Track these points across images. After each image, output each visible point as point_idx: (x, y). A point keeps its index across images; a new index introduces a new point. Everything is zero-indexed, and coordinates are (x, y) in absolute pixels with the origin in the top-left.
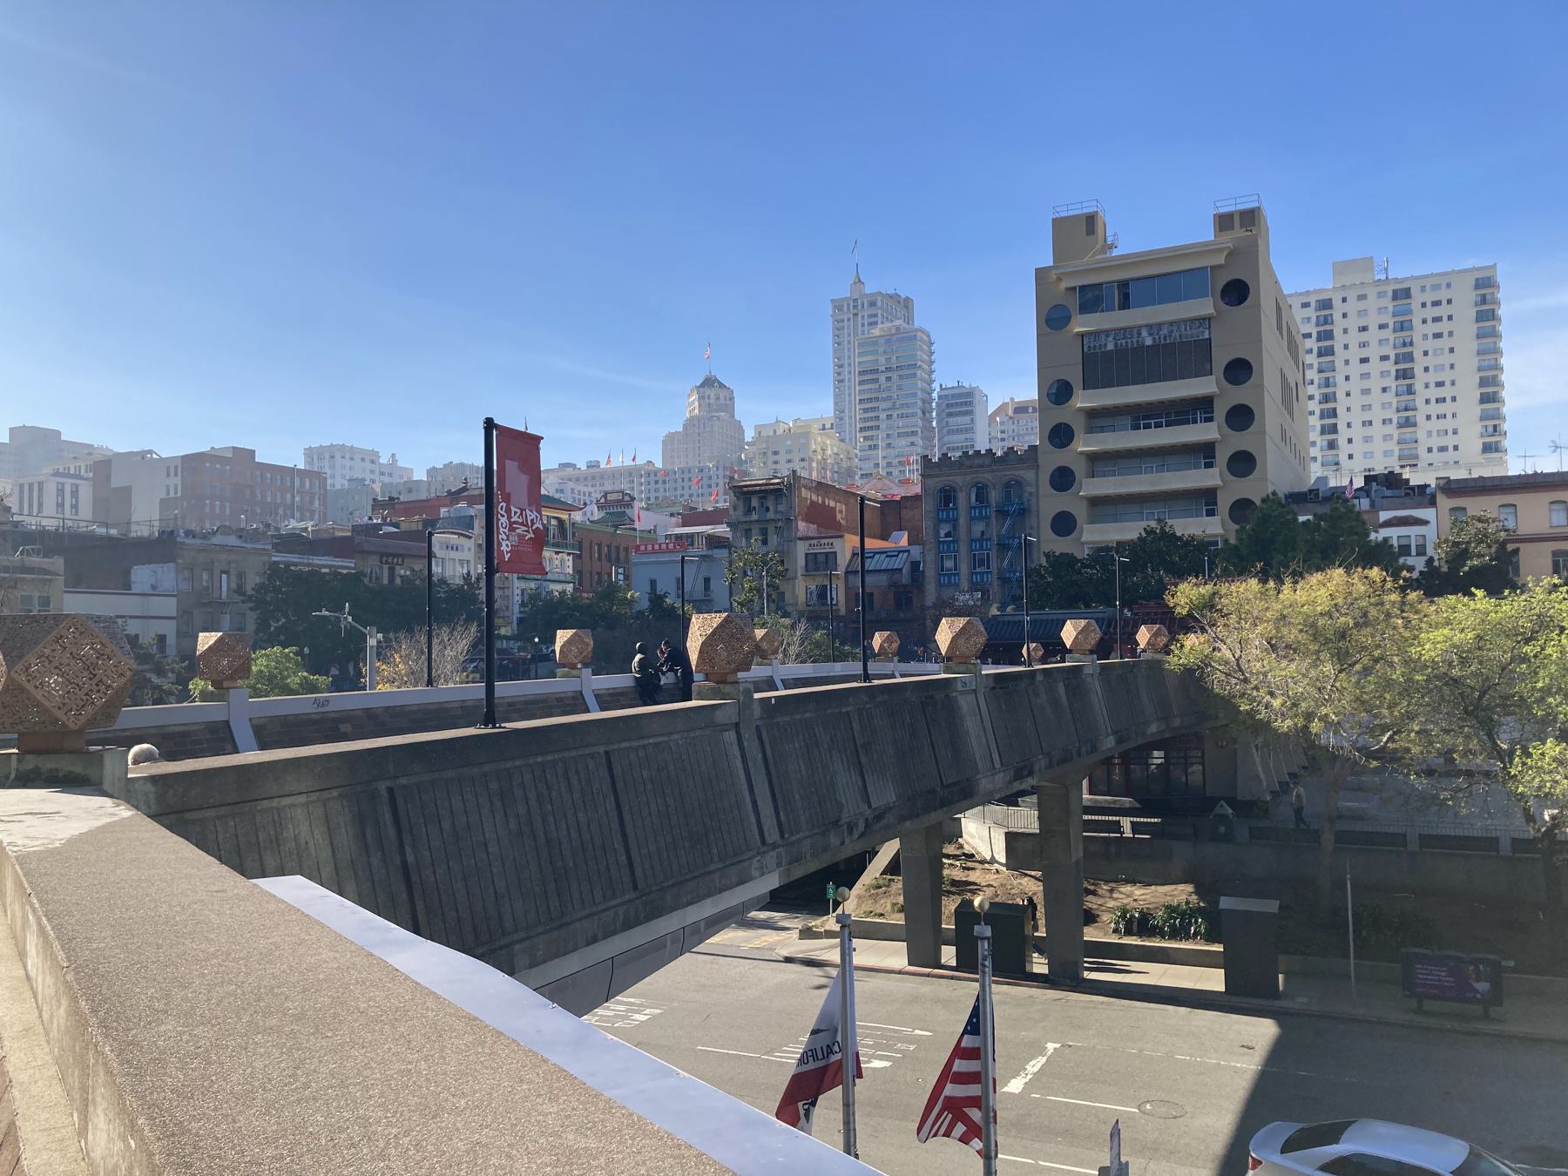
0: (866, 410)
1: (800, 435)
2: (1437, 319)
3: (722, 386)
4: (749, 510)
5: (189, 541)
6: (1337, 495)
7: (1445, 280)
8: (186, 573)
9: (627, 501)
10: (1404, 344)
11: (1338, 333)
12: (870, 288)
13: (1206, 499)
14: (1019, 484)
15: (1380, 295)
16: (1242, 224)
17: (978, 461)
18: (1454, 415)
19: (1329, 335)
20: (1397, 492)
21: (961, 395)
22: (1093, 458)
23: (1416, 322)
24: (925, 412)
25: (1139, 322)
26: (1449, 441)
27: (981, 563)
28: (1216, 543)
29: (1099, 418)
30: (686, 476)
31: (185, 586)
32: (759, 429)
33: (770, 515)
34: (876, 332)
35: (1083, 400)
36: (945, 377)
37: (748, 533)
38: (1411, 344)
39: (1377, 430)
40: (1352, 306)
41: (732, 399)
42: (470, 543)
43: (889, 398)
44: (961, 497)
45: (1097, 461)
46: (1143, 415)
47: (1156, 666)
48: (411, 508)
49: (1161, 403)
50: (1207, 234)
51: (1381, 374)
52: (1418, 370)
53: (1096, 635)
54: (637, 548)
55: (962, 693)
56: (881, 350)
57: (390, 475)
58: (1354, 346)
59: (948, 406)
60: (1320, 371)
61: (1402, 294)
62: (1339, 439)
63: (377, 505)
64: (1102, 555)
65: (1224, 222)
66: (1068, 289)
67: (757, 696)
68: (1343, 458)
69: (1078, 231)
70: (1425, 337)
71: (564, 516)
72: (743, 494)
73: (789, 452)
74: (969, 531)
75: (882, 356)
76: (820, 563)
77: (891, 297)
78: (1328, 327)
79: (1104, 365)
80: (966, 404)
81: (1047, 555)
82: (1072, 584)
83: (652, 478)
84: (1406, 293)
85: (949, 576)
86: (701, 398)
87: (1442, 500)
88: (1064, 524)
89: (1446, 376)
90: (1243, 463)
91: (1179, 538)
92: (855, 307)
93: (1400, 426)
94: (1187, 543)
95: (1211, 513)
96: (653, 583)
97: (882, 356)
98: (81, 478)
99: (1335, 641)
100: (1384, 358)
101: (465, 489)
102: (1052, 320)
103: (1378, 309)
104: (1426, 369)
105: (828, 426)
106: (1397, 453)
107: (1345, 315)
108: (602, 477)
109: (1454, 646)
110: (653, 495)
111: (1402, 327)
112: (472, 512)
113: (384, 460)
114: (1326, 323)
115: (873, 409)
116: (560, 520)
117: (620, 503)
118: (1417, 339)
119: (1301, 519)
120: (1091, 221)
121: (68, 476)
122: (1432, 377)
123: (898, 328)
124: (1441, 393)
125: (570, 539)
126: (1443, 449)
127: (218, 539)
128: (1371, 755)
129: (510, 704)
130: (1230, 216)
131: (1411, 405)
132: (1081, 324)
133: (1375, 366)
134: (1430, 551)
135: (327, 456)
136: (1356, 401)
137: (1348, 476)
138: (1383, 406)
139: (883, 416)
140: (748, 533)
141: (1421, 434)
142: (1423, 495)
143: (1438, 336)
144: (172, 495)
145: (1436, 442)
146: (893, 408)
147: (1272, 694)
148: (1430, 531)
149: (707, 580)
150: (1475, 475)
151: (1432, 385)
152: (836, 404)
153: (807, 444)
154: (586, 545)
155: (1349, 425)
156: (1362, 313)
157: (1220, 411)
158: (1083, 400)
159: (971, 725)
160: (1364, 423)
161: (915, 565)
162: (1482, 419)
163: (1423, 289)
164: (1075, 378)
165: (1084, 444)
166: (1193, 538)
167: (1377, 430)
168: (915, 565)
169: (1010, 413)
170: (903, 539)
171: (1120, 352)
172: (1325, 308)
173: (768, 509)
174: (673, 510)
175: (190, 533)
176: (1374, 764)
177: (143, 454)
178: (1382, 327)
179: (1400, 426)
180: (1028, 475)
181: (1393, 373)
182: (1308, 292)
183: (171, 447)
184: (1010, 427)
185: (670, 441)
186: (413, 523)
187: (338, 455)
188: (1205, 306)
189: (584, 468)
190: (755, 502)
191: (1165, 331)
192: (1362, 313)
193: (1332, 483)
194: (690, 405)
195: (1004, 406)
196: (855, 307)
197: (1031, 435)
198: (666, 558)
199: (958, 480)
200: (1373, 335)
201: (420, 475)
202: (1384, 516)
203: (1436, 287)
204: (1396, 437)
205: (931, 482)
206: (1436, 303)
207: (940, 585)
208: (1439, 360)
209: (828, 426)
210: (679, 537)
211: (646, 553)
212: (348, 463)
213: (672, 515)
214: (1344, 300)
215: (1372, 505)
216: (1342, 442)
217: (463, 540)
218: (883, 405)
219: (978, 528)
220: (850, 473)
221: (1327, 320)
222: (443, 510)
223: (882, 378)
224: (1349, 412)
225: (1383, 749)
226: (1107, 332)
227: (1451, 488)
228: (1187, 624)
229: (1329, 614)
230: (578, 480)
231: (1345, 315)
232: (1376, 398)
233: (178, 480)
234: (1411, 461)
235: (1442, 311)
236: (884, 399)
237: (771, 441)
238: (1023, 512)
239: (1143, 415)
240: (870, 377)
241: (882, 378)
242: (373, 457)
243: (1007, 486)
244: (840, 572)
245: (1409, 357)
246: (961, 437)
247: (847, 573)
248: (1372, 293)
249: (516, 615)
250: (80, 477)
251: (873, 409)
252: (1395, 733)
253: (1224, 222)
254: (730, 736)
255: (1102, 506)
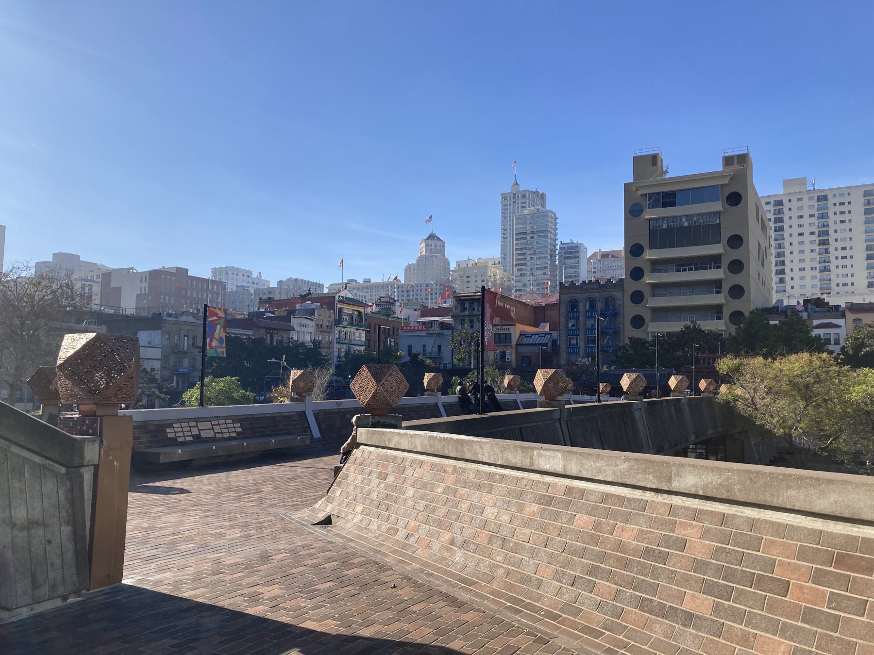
0: (519, 255)
1: (481, 267)
2: (842, 213)
3: (438, 239)
4: (464, 309)
5: (169, 319)
6: (792, 308)
7: (847, 191)
8: (167, 336)
9: (391, 302)
10: (824, 226)
11: (786, 218)
12: (522, 188)
13: (717, 311)
14: (613, 299)
15: (810, 198)
16: (738, 163)
17: (590, 286)
18: (852, 266)
19: (781, 220)
20: (822, 309)
21: (572, 247)
22: (654, 286)
23: (831, 214)
24: (552, 256)
25: (682, 213)
26: (849, 280)
27: (592, 342)
28: (722, 335)
29: (657, 265)
30: (419, 289)
31: (166, 343)
32: (458, 264)
33: (475, 312)
34: (526, 212)
35: (650, 255)
36: (564, 237)
37: (462, 322)
38: (828, 226)
39: (808, 273)
40: (795, 204)
41: (444, 246)
42: (312, 323)
43: (532, 248)
44: (581, 305)
45: (658, 289)
46: (682, 264)
47: (710, 401)
48: (280, 304)
49: (692, 257)
50: (718, 167)
51: (810, 242)
52: (832, 241)
53: (643, 383)
54: (402, 328)
55: (637, 410)
56: (528, 222)
57: (258, 284)
58: (795, 226)
59: (565, 253)
60: (776, 240)
61: (823, 198)
62: (790, 279)
63: (262, 302)
64: (659, 340)
65: (728, 161)
66: (642, 195)
67: (567, 407)
68: (788, 288)
69: (647, 164)
70: (836, 222)
71: (362, 310)
72: (461, 300)
73: (476, 276)
74: (585, 324)
75: (528, 225)
76: (502, 339)
77: (534, 193)
78: (780, 216)
79: (661, 236)
80: (575, 252)
81: (630, 339)
82: (637, 356)
83: (400, 290)
84: (825, 198)
85: (574, 348)
86: (427, 246)
87: (848, 314)
88: (638, 322)
89: (847, 244)
90: (737, 292)
91: (704, 332)
92: (514, 198)
93: (821, 271)
94: (708, 334)
95: (719, 318)
96: (410, 347)
97: (528, 225)
98: (94, 282)
99: (803, 390)
100: (812, 233)
101: (309, 294)
102: (633, 211)
103: (809, 206)
104: (836, 240)
105: (497, 262)
106: (819, 286)
107: (790, 209)
108: (372, 288)
109: (868, 394)
110: (405, 298)
111: (823, 216)
112: (313, 307)
113: (254, 276)
114: (779, 213)
115: (523, 254)
116: (359, 312)
117: (388, 303)
118: (831, 223)
119: (772, 323)
120: (654, 159)
121: (87, 280)
122: (840, 245)
123: (538, 210)
124: (844, 253)
125: (364, 323)
126: (845, 285)
127: (184, 318)
128: (823, 449)
129: (410, 408)
130: (732, 157)
131: (827, 259)
132: (649, 214)
133: (807, 238)
134: (842, 343)
135: (224, 273)
136: (796, 256)
137: (792, 299)
138: (811, 260)
139: (529, 258)
140: (462, 322)
141: (833, 276)
142: (837, 312)
143: (843, 222)
144: (143, 292)
145: (842, 281)
146: (535, 253)
147: (772, 417)
148: (843, 330)
149: (439, 347)
150: (867, 301)
151: (839, 249)
152: (502, 251)
153: (486, 272)
154: (372, 326)
155: (792, 270)
156: (800, 208)
157: (725, 263)
158: (650, 255)
159: (640, 424)
160: (800, 269)
161: (554, 342)
162: (868, 268)
163: (835, 195)
164: (645, 242)
165: (649, 279)
166: (710, 331)
167: (808, 273)
168: (554, 342)
169: (599, 257)
170: (547, 327)
171: (670, 229)
172: (779, 205)
173: (474, 309)
174: (415, 307)
175: (169, 315)
176: (825, 454)
177: (128, 270)
178: (811, 216)
179: (821, 271)
180: (619, 295)
181: (817, 242)
182: (769, 196)
183: (143, 266)
184: (598, 265)
185: (409, 269)
186: (282, 312)
187: (230, 273)
188: (717, 206)
189: (362, 282)
190: (467, 305)
191: (695, 219)
192: (800, 208)
193: (786, 304)
194: (420, 249)
195: (595, 254)
196: (514, 198)
197: (619, 272)
198: (418, 334)
199: (579, 296)
200: (806, 220)
201: (274, 284)
202: (816, 322)
203: (842, 195)
204: (818, 277)
205: (565, 297)
206: (842, 204)
207: (568, 353)
208: (843, 235)
209: (497, 262)
210: (424, 323)
211: (407, 331)
212: (235, 277)
213: (415, 310)
214: (790, 201)
215: (809, 316)
216: (788, 279)
217: (309, 322)
218: (528, 252)
219: (590, 322)
220: (509, 289)
221: (780, 212)
222: (298, 305)
223: (529, 237)
224: (792, 263)
225: (827, 447)
226: (663, 219)
227: (854, 308)
228: (726, 379)
229: (800, 376)
230: (358, 289)
231: (790, 209)
232: (807, 255)
233: (147, 285)
234: (827, 291)
235: (846, 208)
236: (529, 249)
237: (466, 271)
238: (615, 315)
239: (682, 264)
240: (522, 236)
241: (529, 237)
242: (248, 274)
243: (607, 300)
244: (514, 343)
245: (827, 233)
246: (572, 271)
247: (517, 344)
248: (805, 197)
249: (335, 362)
250: (94, 282)
251: (523, 254)
252: (834, 439)
253: (728, 161)
254: (558, 424)
255: (660, 313)
